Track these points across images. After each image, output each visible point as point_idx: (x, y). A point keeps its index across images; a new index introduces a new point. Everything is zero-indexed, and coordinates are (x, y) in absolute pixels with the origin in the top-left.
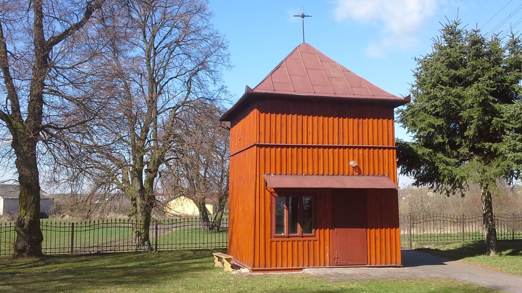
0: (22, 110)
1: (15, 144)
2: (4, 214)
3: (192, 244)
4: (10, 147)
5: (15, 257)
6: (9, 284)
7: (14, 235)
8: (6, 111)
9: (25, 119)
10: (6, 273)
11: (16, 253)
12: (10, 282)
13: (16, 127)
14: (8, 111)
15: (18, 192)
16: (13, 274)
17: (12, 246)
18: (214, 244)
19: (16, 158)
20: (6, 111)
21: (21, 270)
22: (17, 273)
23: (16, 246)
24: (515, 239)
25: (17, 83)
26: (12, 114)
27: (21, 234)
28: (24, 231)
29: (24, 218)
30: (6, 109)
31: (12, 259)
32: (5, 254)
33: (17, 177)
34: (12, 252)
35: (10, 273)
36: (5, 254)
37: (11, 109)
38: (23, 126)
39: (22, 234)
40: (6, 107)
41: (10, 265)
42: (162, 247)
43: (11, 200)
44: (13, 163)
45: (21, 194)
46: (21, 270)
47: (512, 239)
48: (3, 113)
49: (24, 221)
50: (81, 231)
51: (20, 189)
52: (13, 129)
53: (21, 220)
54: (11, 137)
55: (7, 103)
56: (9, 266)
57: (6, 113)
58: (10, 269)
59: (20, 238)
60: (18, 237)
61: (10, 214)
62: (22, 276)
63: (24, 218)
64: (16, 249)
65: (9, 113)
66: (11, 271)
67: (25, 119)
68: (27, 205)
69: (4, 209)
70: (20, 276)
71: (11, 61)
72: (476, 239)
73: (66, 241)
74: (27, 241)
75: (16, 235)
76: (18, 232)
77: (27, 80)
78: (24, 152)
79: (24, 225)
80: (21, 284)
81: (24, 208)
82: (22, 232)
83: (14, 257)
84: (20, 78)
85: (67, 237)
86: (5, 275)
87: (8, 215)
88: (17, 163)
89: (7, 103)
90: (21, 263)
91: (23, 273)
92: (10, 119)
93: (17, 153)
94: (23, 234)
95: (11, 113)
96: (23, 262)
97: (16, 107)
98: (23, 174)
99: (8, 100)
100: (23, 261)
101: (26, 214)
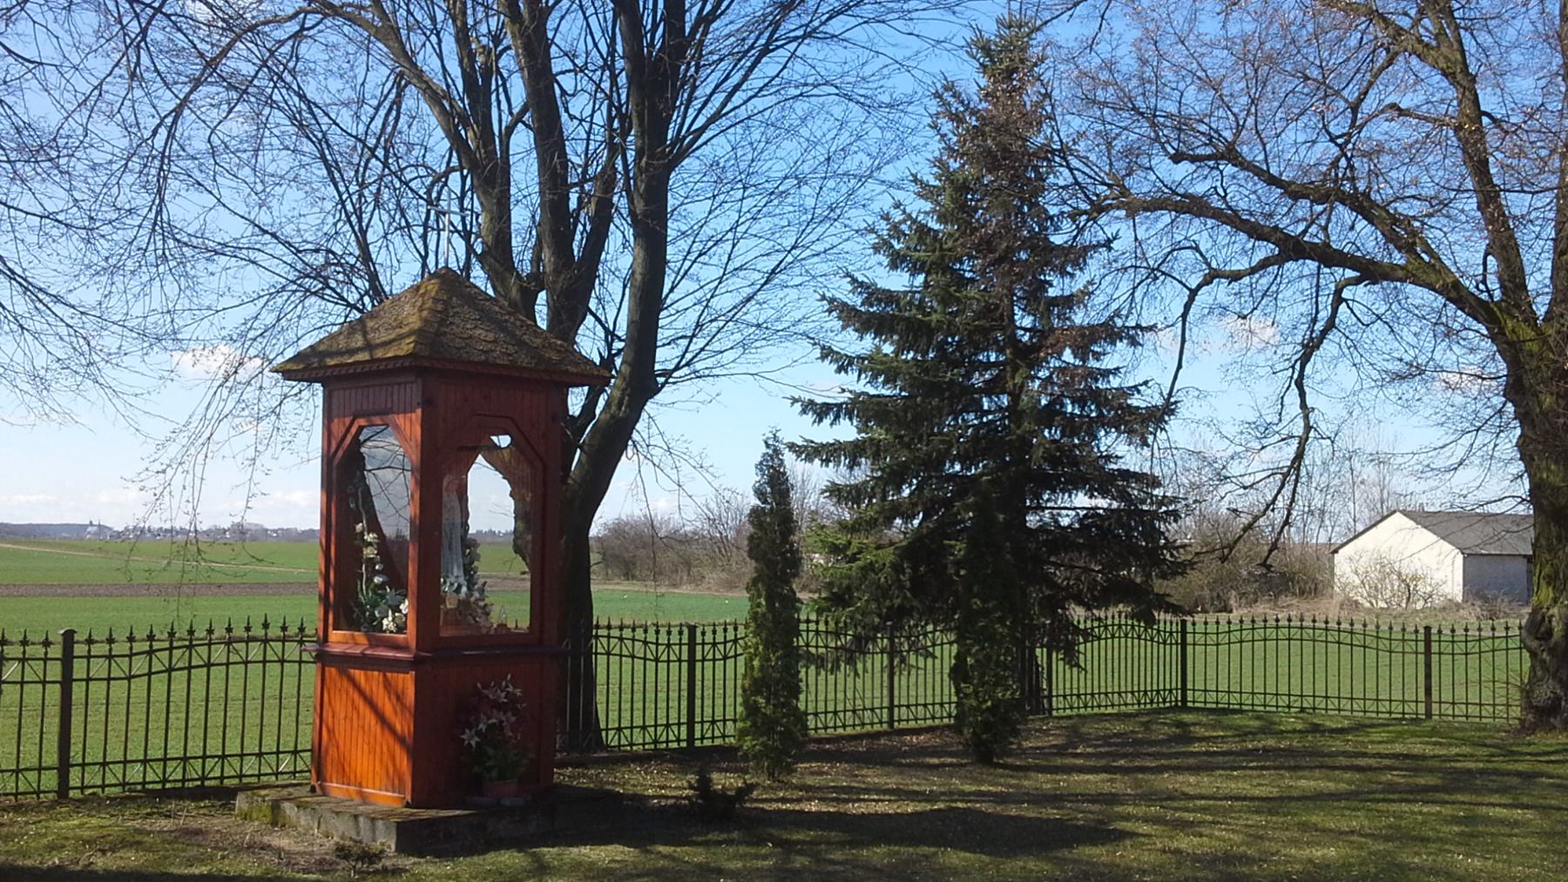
0: (1531, 285)
1: (1516, 389)
2: (1465, 600)
3: (1391, 701)
4: (1498, 401)
5: (1525, 728)
6: (1526, 807)
7: (1521, 664)
8: (1482, 292)
9: (1541, 310)
10: (1509, 773)
11: (1530, 716)
12: (1525, 800)
13: (1515, 339)
14: (1488, 291)
15: (1532, 534)
16: (1528, 777)
17: (1516, 695)
18: (157, 667)
19: (1518, 432)
20: (1482, 292)
21: (1550, 769)
22: (1542, 775)
23: (1527, 692)
24: (698, 743)
25: (1516, 203)
26: (1502, 300)
27: (1544, 661)
28: (1551, 651)
29: (1551, 612)
30: (1482, 287)
31: (1519, 731)
32: (1494, 718)
33: (1522, 489)
34: (1516, 712)
35: (1519, 774)
36: (1494, 718)
37: (1498, 286)
38: (1540, 333)
39: (1545, 661)
40: (1484, 282)
41: (1514, 749)
42: (1200, 696)
43: (1485, 558)
44: (1509, 445)
45: (1537, 539)
46: (1550, 769)
47: (684, 744)
48: (1477, 298)
49: (1550, 622)
50: (1507, 649)
51: (1534, 525)
52: (1509, 348)
53: (1539, 617)
54: (1502, 366)
55: (1485, 269)
56: (1513, 753)
57: (1484, 296)
58: (1516, 761)
59: (1539, 673)
60: (1533, 668)
61: (1485, 600)
62: (1559, 786)
63: (1551, 612)
64: (1529, 704)
65: (1491, 296)
66: (1521, 767)
67: (1541, 310)
68: (1557, 573)
69: (1464, 585)
70: (1551, 785)
71: (1493, 138)
72: (1352, 711)
73: (1410, 679)
74: (1561, 681)
75: (1527, 665)
76: (1533, 655)
77: (1548, 189)
78: (1545, 414)
79: (1550, 632)
80: (1559, 809)
81: (1549, 584)
82: (1545, 655)
83: (1523, 727)
84: (1526, 189)
85: (1410, 671)
86: (1506, 778)
87: (1479, 603)
88: (1523, 445)
89: (1485, 269)
90: (1547, 745)
91: (1559, 777)
92: (1498, 313)
93: (1523, 417)
94: (1548, 659)
95: (1497, 295)
96: (1551, 745)
97: (1514, 278)
98: (1541, 478)
99: (1490, 258)
100: (1554, 741)
101: (1555, 601)
